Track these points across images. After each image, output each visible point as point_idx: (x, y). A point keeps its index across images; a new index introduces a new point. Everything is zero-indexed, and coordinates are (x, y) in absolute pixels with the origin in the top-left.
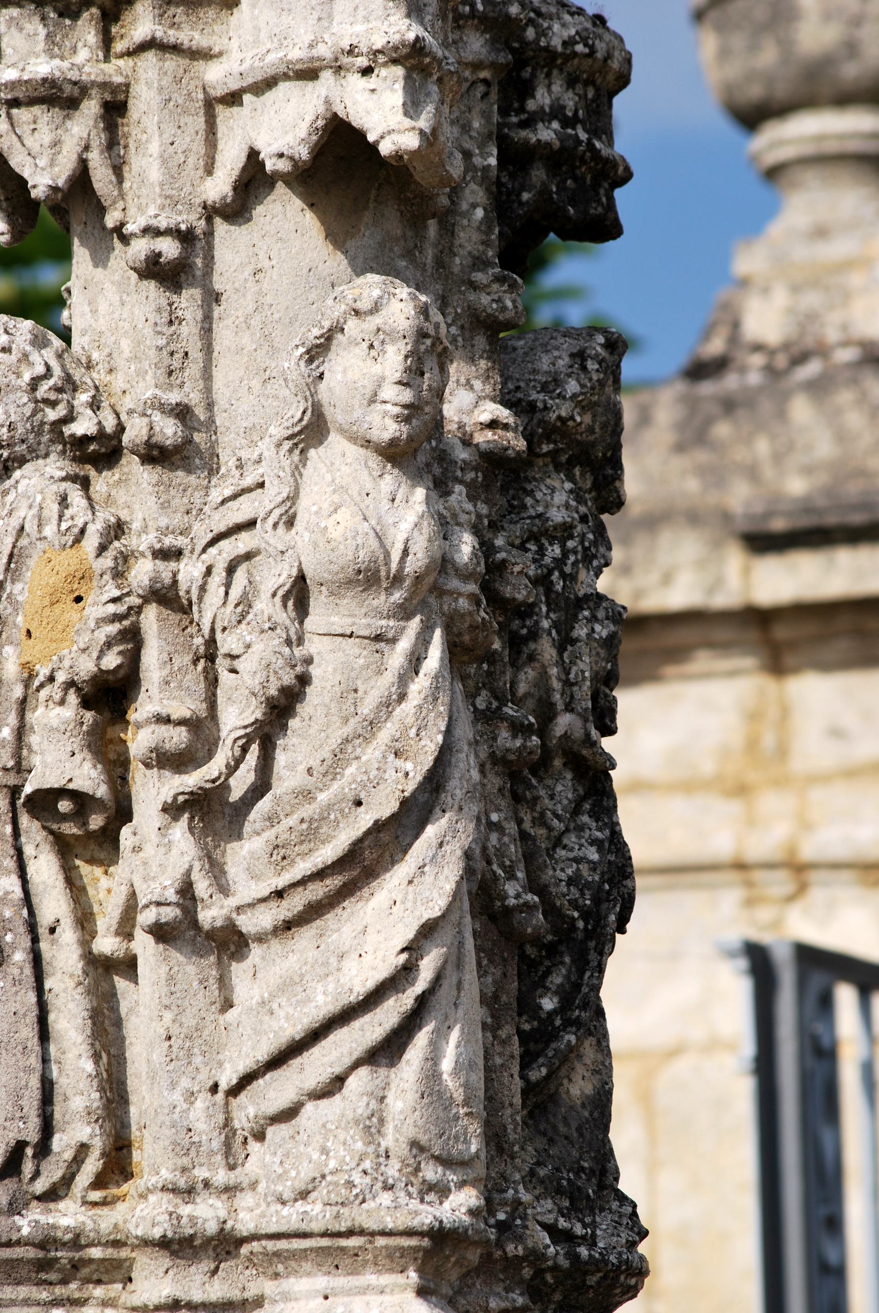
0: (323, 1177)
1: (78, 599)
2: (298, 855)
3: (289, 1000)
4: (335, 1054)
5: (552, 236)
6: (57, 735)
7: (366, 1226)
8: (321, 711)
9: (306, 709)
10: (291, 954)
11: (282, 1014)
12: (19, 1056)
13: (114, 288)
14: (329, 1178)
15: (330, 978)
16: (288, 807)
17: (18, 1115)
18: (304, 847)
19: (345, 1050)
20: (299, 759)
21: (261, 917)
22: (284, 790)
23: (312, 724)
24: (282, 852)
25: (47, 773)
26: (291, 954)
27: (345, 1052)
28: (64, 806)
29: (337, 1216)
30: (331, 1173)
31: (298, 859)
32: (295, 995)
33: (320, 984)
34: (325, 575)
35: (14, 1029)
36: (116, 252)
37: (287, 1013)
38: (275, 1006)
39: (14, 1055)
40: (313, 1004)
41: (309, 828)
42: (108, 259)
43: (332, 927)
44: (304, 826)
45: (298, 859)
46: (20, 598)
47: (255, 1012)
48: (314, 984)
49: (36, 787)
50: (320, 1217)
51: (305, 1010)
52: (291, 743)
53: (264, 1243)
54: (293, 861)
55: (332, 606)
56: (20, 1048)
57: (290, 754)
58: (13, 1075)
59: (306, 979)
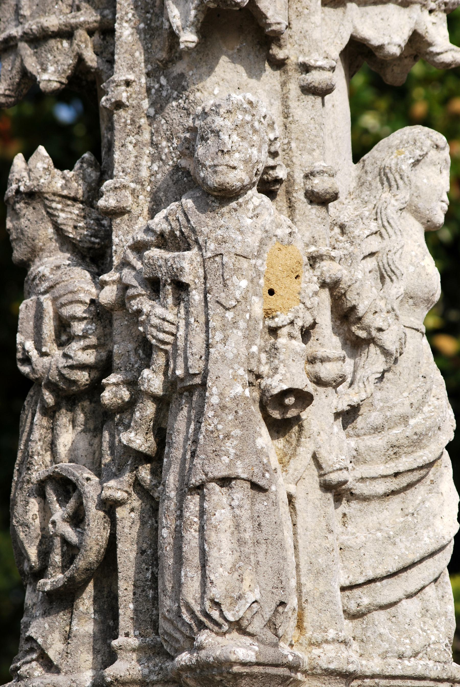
0: (429, 645)
1: (297, 277)
2: (405, 453)
3: (407, 538)
4: (426, 573)
5: (102, 86)
6: (298, 357)
7: (457, 677)
8: (406, 371)
9: (398, 368)
10: (385, 511)
11: (401, 545)
12: (279, 550)
13: (265, 94)
14: (432, 646)
15: (430, 529)
16: (392, 424)
17: (280, 586)
18: (410, 449)
19: (431, 571)
20: (391, 397)
21: (377, 486)
22: (395, 414)
23: (401, 378)
24: (396, 450)
25: (296, 379)
26: (385, 511)
27: (431, 573)
28: (290, 400)
29: (444, 669)
30: (434, 643)
31: (403, 456)
32: (411, 536)
33: (425, 531)
34: (419, 293)
35: (275, 533)
36: (267, 73)
37: (406, 546)
38: (397, 540)
39: (277, 549)
40: (423, 542)
41: (418, 439)
42: (261, 76)
43: (409, 498)
44: (415, 437)
45: (403, 456)
46: (261, 269)
47: (381, 542)
48: (422, 531)
49: (290, 387)
50: (435, 669)
51: (418, 545)
52: (386, 386)
53: (377, 680)
54: (400, 456)
55: (412, 311)
56: (279, 544)
57: (384, 393)
58: (277, 561)
59: (417, 527)
